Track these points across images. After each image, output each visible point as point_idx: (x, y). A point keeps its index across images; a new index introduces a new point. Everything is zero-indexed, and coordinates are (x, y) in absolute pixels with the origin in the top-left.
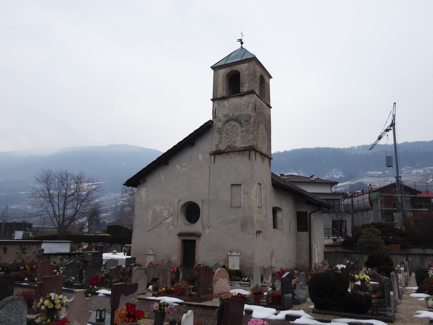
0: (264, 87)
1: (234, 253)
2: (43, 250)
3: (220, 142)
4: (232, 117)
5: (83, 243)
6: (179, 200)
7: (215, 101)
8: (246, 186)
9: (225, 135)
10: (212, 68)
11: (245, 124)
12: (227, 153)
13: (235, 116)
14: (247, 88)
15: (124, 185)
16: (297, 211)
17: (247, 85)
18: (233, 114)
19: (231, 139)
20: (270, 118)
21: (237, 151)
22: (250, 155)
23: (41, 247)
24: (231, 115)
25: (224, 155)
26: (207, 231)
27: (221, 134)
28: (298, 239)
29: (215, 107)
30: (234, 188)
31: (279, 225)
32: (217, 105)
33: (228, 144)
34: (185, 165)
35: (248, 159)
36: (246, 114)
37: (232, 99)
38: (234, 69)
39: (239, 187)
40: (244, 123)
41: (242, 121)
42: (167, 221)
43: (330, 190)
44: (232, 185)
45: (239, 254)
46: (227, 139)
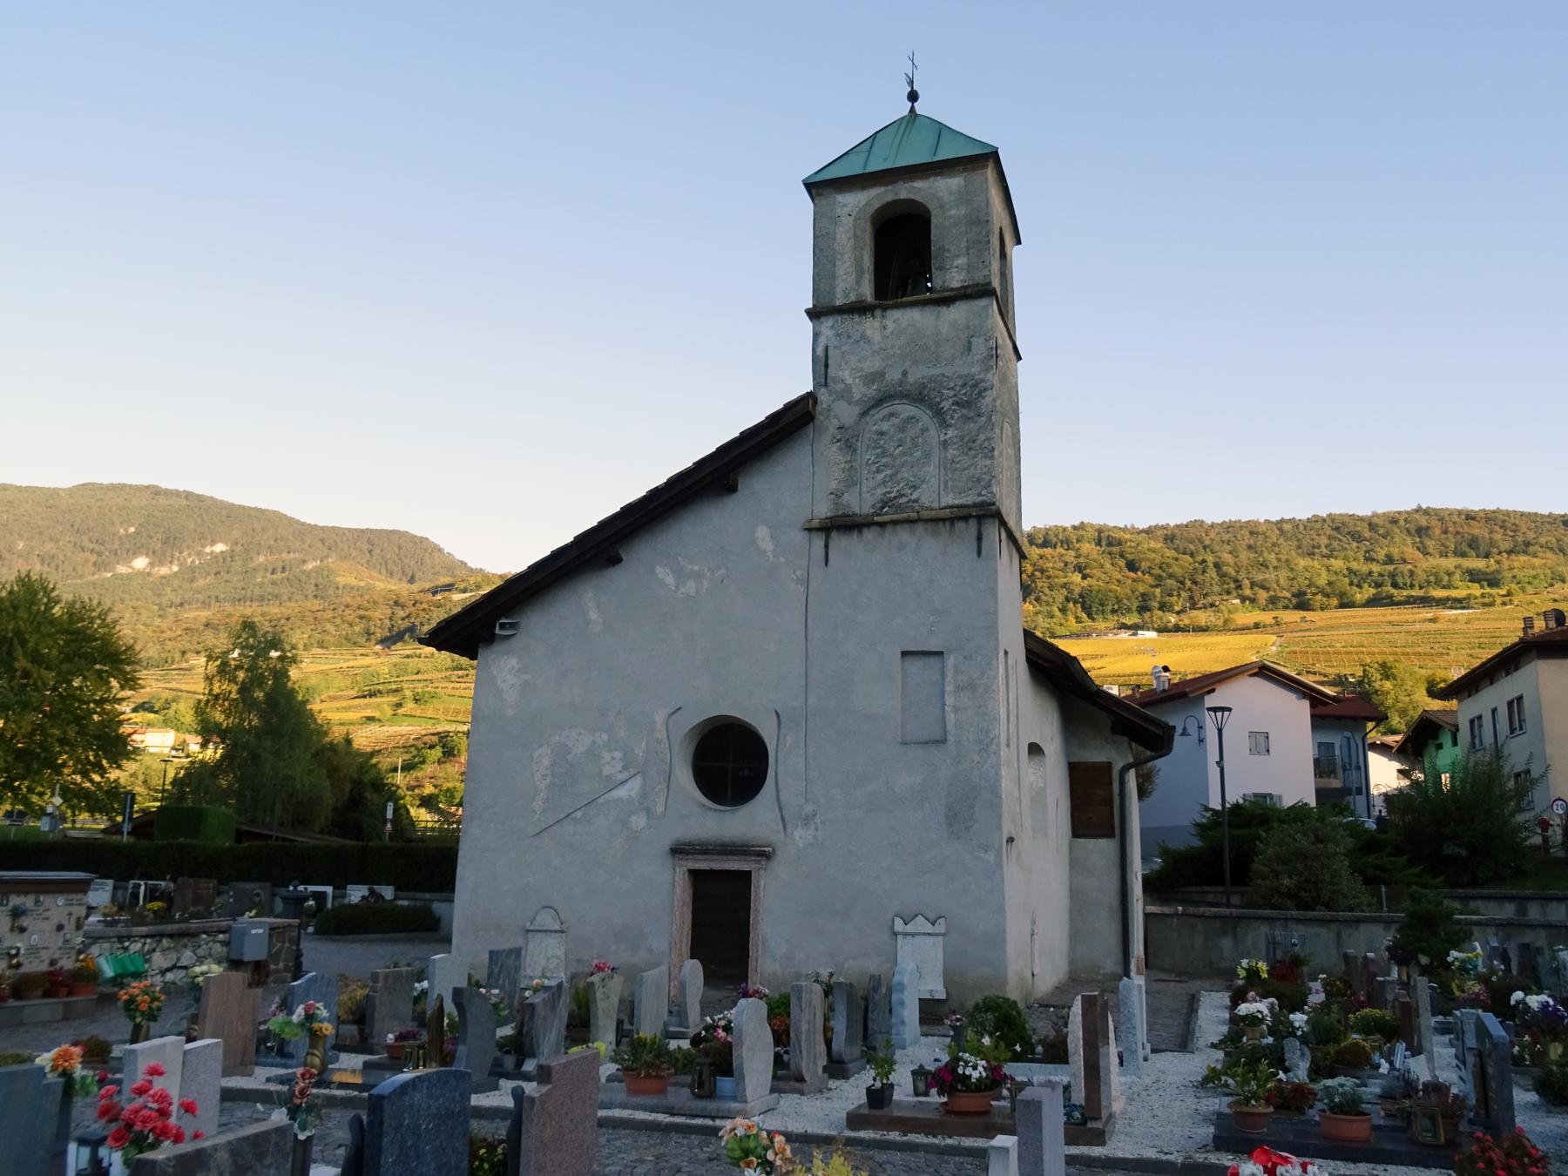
1: (920, 925)
3: (851, 480)
8: (965, 658)
9: (869, 456)
12: (882, 525)
13: (911, 379)
16: (1075, 759)
17: (962, 261)
18: (905, 373)
19: (898, 472)
22: (979, 539)
24: (894, 375)
25: (869, 534)
26: (801, 836)
29: (822, 341)
30: (916, 665)
32: (830, 333)
34: (696, 568)
35: (975, 555)
36: (960, 376)
38: (903, 195)
39: (933, 661)
40: (955, 411)
41: (946, 405)
42: (621, 793)
44: (904, 654)
46: (878, 471)
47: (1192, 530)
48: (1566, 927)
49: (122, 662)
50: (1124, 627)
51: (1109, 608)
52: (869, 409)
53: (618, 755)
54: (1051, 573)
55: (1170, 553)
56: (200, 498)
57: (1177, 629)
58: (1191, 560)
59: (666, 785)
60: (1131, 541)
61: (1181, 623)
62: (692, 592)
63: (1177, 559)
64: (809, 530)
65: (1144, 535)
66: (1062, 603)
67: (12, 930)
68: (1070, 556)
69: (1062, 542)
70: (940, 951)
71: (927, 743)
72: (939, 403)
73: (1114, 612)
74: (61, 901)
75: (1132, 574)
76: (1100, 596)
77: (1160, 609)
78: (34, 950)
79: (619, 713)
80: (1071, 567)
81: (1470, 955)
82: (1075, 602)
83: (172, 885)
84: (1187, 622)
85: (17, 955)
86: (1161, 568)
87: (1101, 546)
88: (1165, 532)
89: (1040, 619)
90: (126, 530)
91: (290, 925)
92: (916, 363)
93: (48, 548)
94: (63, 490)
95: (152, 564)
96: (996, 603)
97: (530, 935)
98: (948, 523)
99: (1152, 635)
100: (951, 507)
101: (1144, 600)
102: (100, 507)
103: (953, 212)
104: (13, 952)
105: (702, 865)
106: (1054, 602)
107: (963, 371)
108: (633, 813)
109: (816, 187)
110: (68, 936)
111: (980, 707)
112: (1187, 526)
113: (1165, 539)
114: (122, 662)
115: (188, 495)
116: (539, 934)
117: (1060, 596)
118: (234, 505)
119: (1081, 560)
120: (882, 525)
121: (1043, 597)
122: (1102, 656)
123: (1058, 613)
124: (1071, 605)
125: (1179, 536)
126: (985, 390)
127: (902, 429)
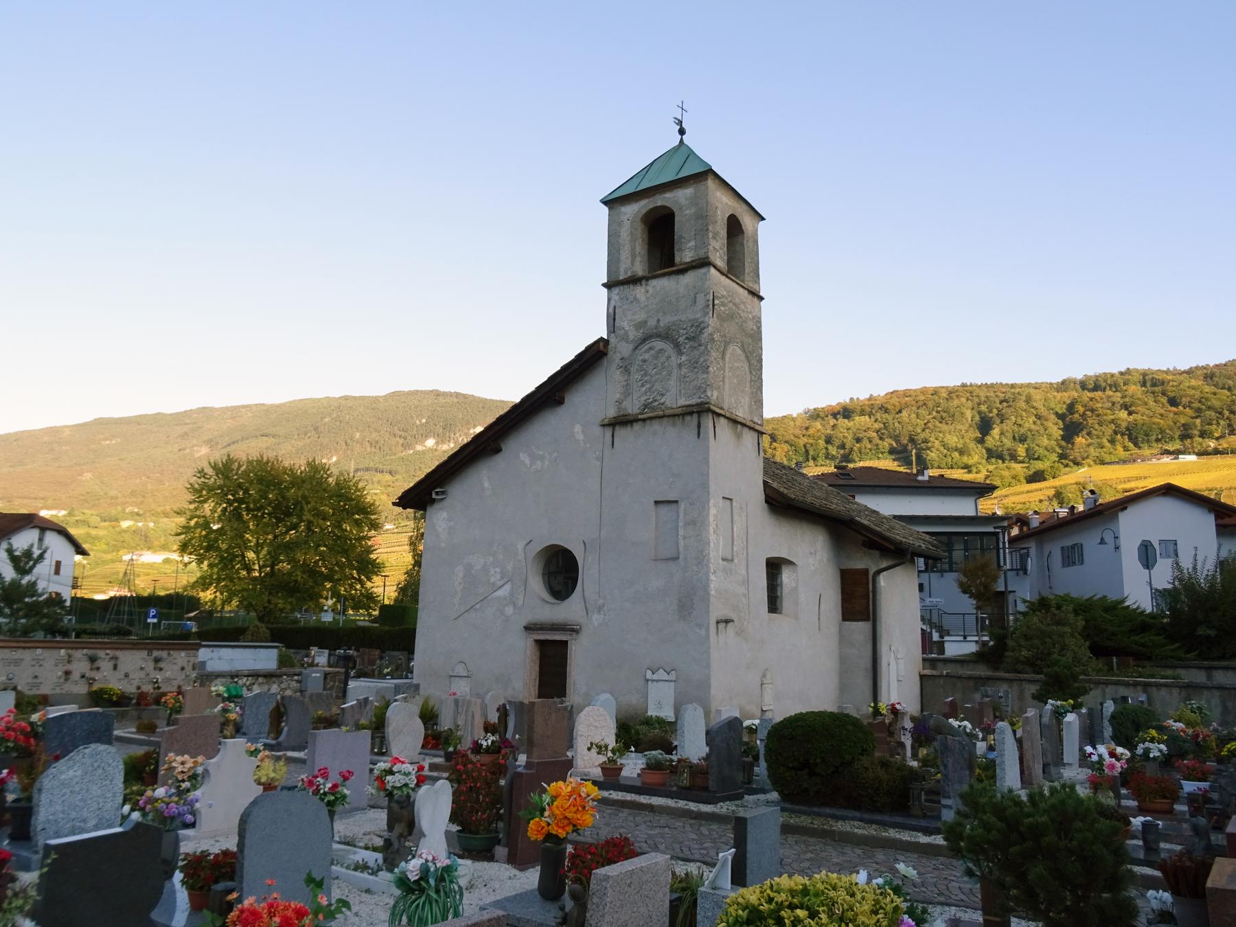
0: (742, 244)
1: (661, 674)
2: (203, 664)
3: (627, 393)
4: (656, 328)
5: (315, 649)
6: (526, 542)
7: (613, 289)
8: (690, 504)
9: (637, 376)
10: (606, 202)
11: (687, 346)
12: (644, 420)
13: (662, 324)
14: (693, 252)
15: (394, 504)
16: (843, 567)
17: (692, 243)
18: (658, 321)
19: (653, 386)
20: (759, 328)
21: (669, 416)
22: (699, 426)
23: (196, 656)
24: (652, 323)
25: (637, 426)
26: (596, 619)
27: (630, 373)
28: (842, 639)
29: (613, 302)
30: (664, 509)
31: (786, 603)
32: (617, 298)
33: (646, 398)
34: (541, 453)
35: (696, 436)
36: (690, 321)
37: (654, 282)
38: (659, 204)
39: (673, 506)
40: (686, 343)
41: (681, 339)
42: (500, 593)
43: (974, 508)
44: (657, 503)
45: (673, 676)
46: (643, 385)
47: (1230, 368)
48: (1234, 688)
49: (368, 513)
50: (1168, 452)
51: (1154, 437)
52: (638, 346)
53: (498, 570)
54: (1100, 412)
55: (1207, 389)
56: (465, 397)
57: (1216, 452)
58: (1229, 394)
59: (523, 588)
60: (1173, 381)
61: (1220, 447)
62: (539, 467)
63: (1215, 394)
64: (603, 426)
65: (1185, 375)
66: (1111, 435)
67: (155, 669)
68: (1117, 397)
69: (1111, 386)
70: (672, 691)
71: (668, 559)
72: (677, 339)
73: (1158, 440)
74: (183, 654)
75: (1174, 409)
76: (1145, 428)
77: (1200, 436)
78: (168, 680)
79: (499, 544)
80: (1118, 406)
81: (1064, 703)
82: (1123, 434)
83: (356, 653)
84: (1225, 446)
85: (157, 682)
86: (1200, 402)
87: (1146, 387)
88: (1205, 371)
89: (1092, 449)
90: (420, 421)
91: (338, 672)
92: (665, 313)
93: (374, 437)
94: (381, 397)
95: (437, 443)
96: (708, 467)
97: (452, 678)
98: (681, 417)
99: (1193, 458)
100: (683, 407)
101: (1186, 429)
102: (404, 407)
103: (687, 212)
104: (155, 680)
105: (542, 637)
106: (1103, 435)
107: (692, 317)
108: (507, 605)
109: (611, 202)
110: (188, 673)
111: (698, 536)
112: (1225, 365)
113: (1205, 378)
114: (368, 513)
115: (457, 395)
116: (457, 678)
117: (1109, 430)
118: (486, 400)
119: (1127, 400)
120: (644, 420)
121: (1094, 432)
122: (1146, 478)
123: (1108, 444)
124: (1119, 437)
125: (1218, 374)
126: (704, 328)
127: (656, 357)
